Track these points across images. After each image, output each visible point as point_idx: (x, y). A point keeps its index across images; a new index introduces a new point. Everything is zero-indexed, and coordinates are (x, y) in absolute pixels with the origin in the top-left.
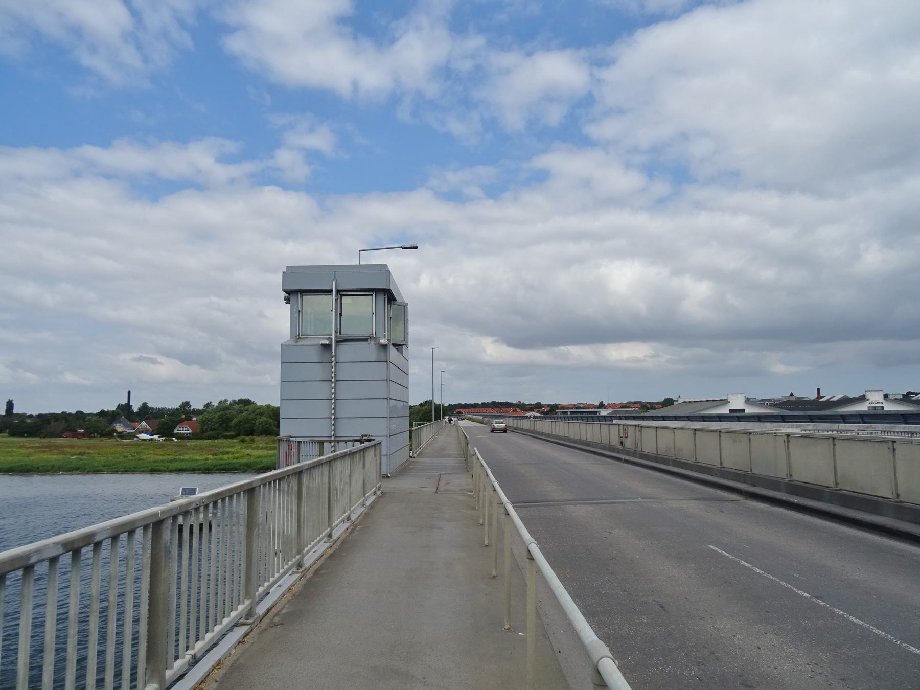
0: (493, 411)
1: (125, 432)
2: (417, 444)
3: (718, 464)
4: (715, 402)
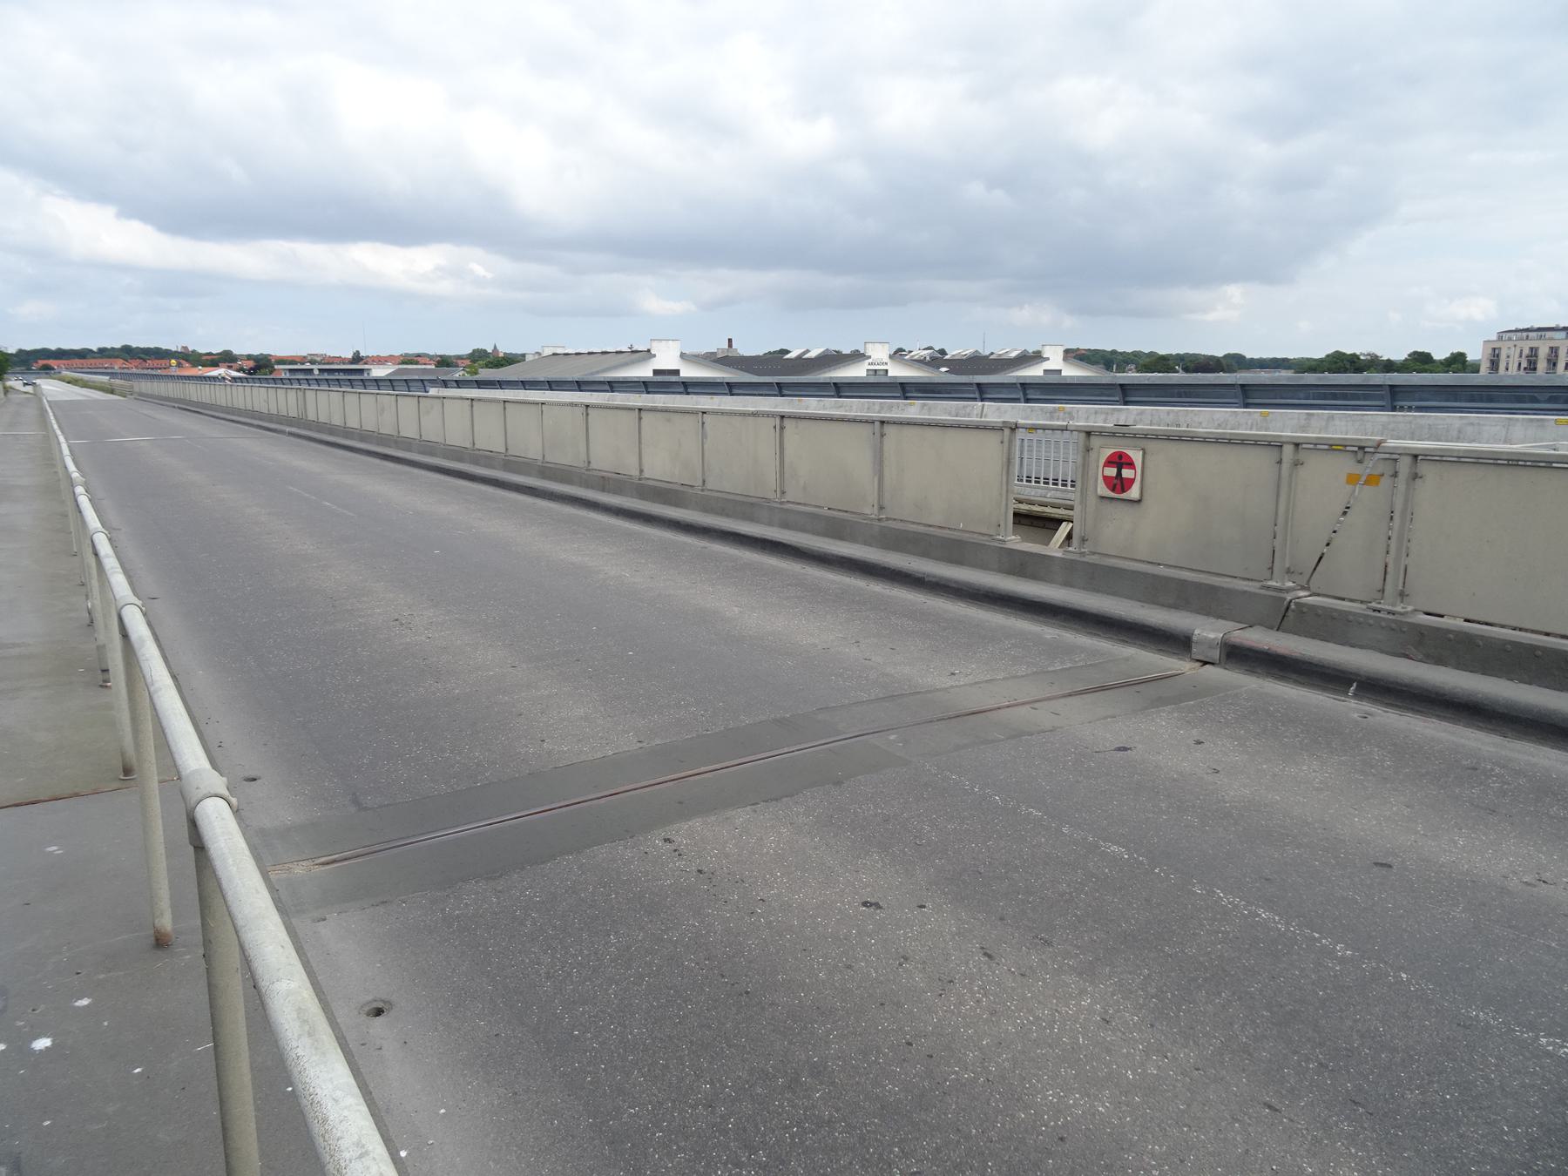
0: (128, 365)
3: (635, 473)
4: (638, 354)
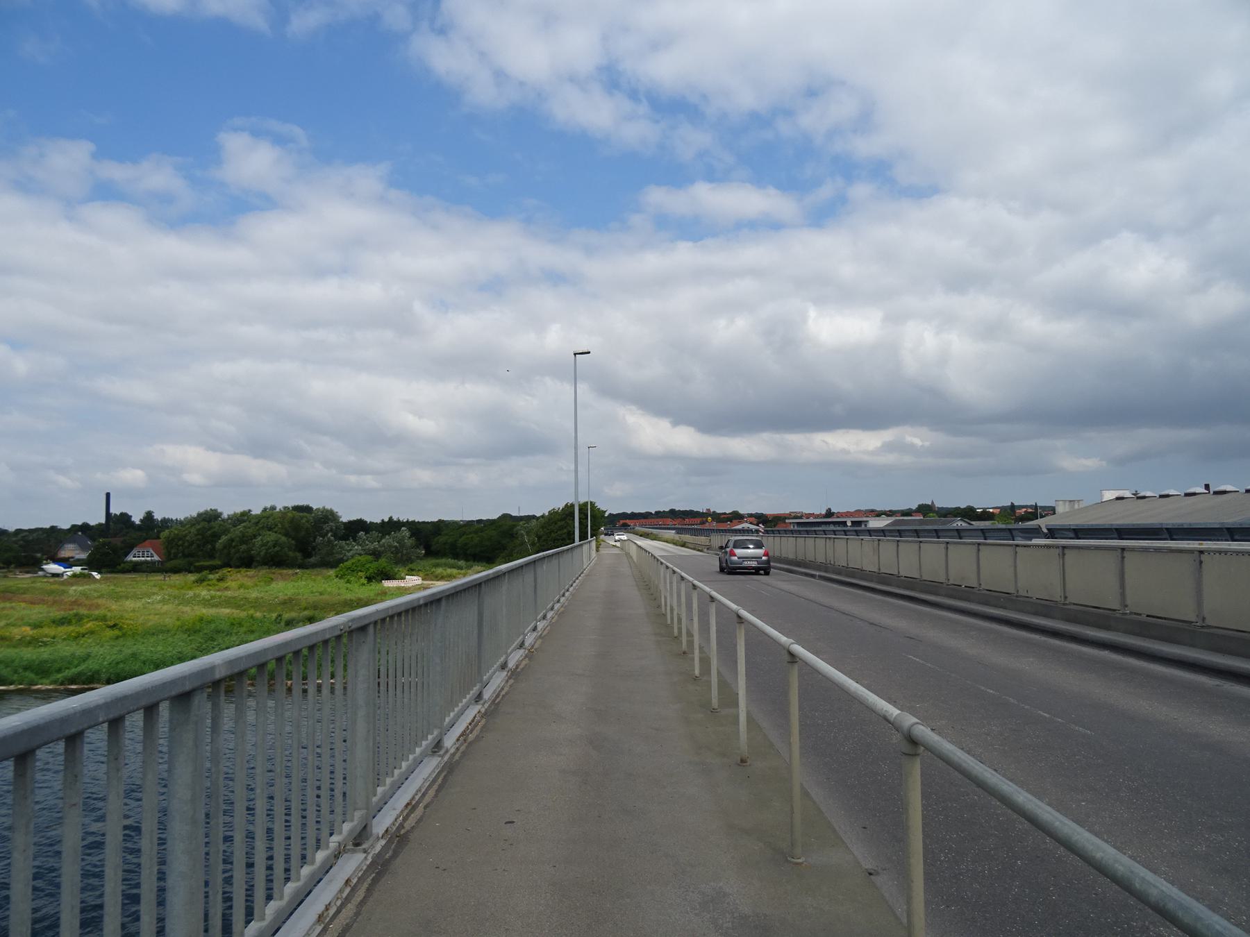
1: (72, 558)
2: (295, 852)
4: (1225, 496)
